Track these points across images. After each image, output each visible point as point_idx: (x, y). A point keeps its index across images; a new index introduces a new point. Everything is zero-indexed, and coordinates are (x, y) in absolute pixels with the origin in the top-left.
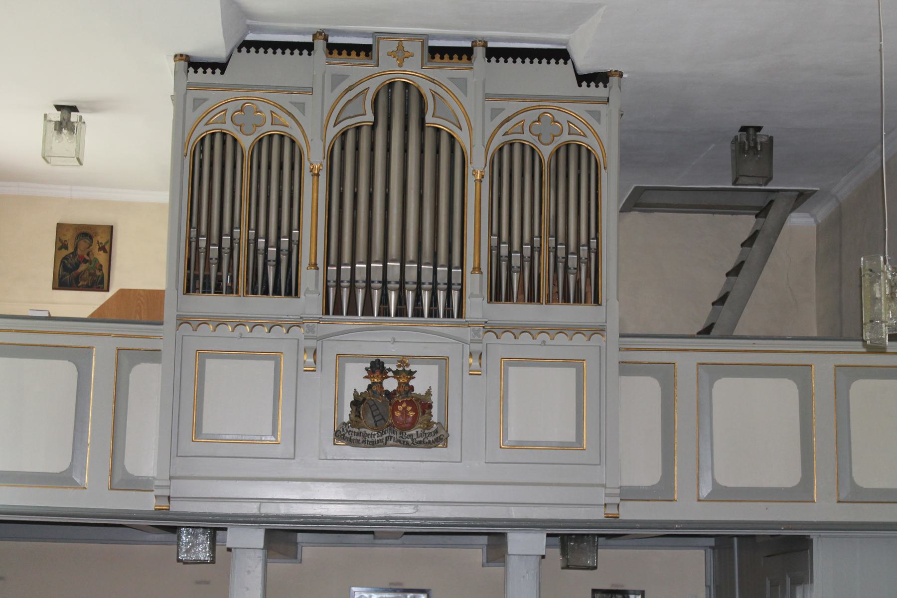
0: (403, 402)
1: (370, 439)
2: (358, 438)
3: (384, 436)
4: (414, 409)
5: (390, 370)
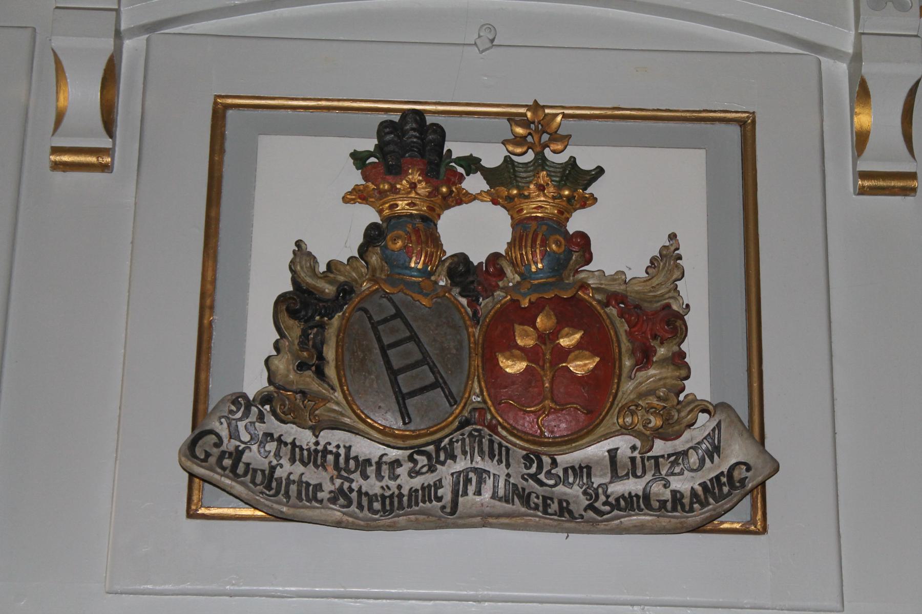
0: (537, 307)
1: (373, 486)
2: (312, 475)
3: (447, 471)
4: (598, 342)
5: (472, 164)
